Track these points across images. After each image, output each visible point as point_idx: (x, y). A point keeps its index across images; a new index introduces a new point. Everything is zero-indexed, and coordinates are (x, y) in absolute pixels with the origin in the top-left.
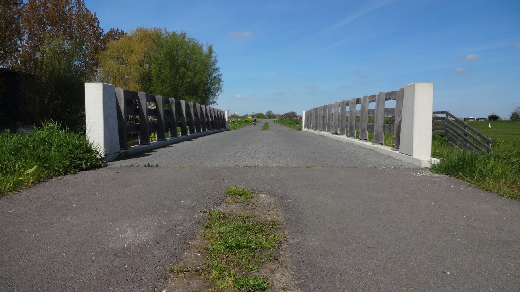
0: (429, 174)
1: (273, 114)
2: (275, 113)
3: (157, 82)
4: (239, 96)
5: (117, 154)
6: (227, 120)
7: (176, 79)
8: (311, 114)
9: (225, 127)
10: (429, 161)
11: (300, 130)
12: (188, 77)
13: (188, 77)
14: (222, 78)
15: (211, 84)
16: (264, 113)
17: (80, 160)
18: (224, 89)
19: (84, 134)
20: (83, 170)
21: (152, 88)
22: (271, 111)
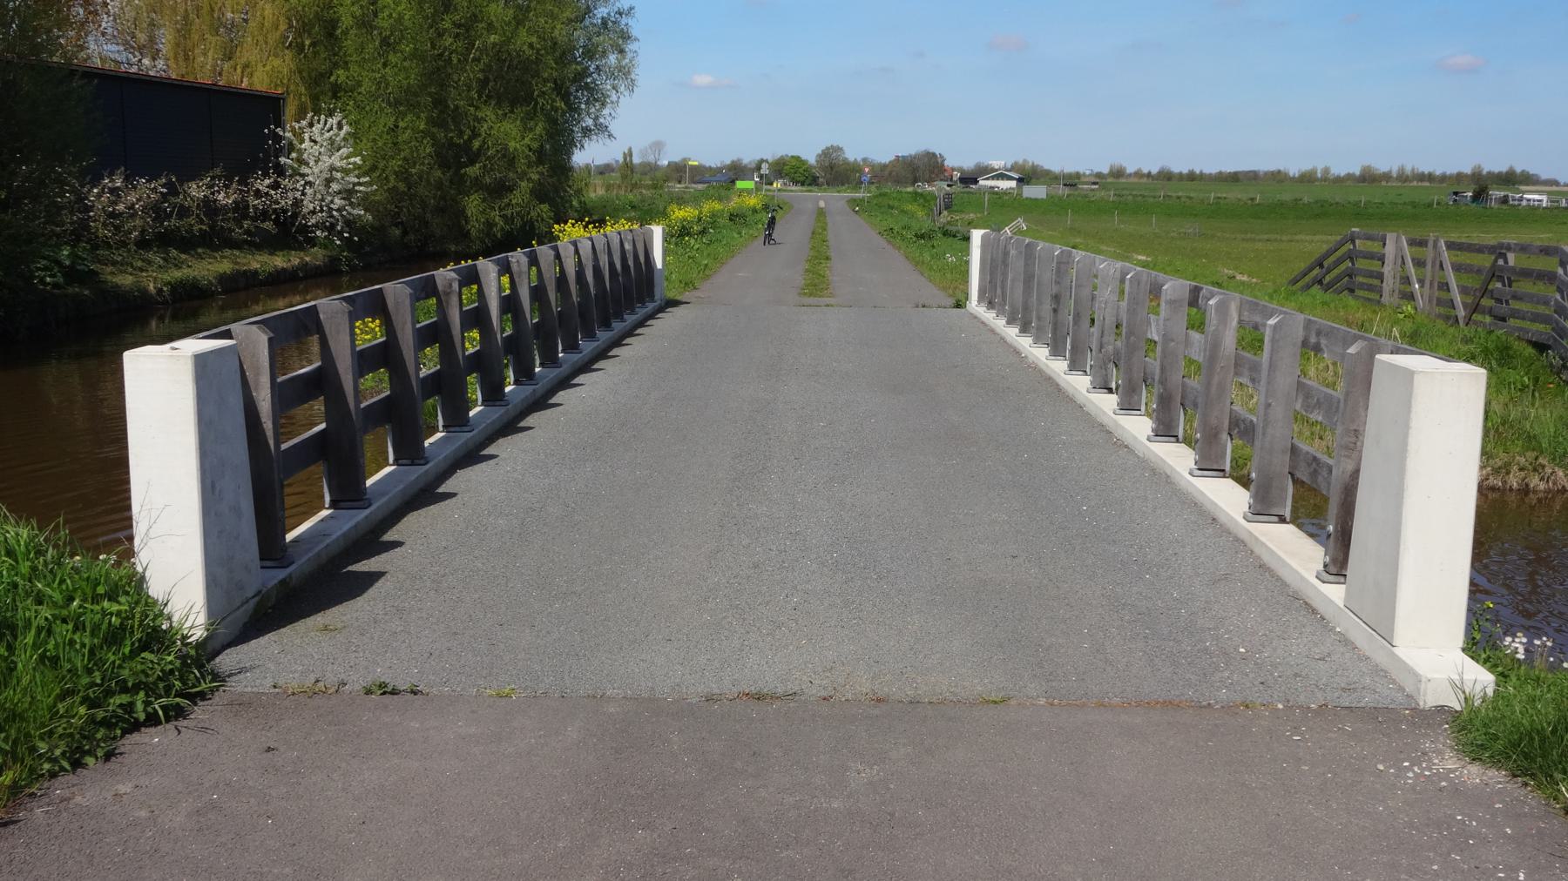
0: (1450, 764)
1: (846, 161)
2: (852, 154)
3: (361, 49)
4: (703, 80)
5: (252, 603)
6: (659, 264)
7: (440, 35)
8: (1006, 254)
9: (650, 294)
10: (1452, 683)
11: (959, 305)
12: (490, 27)
13: (490, 27)
14: (635, 26)
15: (590, 53)
16: (811, 156)
17: (125, 689)
18: (641, 74)
19: (130, 553)
20: (136, 726)
21: (340, 75)
22: (839, 149)
